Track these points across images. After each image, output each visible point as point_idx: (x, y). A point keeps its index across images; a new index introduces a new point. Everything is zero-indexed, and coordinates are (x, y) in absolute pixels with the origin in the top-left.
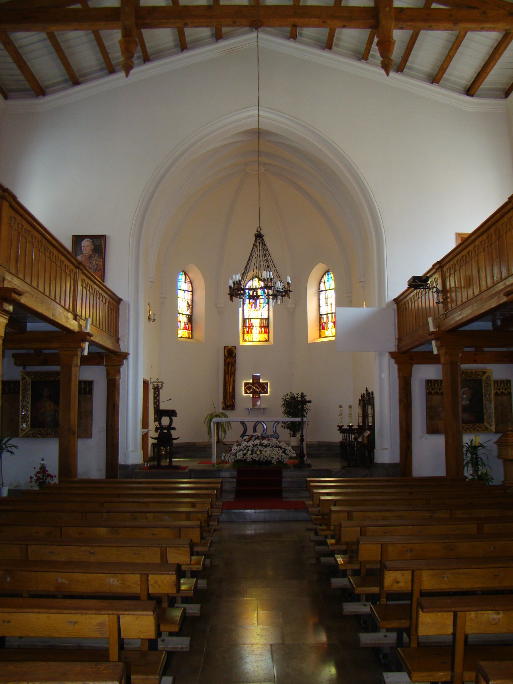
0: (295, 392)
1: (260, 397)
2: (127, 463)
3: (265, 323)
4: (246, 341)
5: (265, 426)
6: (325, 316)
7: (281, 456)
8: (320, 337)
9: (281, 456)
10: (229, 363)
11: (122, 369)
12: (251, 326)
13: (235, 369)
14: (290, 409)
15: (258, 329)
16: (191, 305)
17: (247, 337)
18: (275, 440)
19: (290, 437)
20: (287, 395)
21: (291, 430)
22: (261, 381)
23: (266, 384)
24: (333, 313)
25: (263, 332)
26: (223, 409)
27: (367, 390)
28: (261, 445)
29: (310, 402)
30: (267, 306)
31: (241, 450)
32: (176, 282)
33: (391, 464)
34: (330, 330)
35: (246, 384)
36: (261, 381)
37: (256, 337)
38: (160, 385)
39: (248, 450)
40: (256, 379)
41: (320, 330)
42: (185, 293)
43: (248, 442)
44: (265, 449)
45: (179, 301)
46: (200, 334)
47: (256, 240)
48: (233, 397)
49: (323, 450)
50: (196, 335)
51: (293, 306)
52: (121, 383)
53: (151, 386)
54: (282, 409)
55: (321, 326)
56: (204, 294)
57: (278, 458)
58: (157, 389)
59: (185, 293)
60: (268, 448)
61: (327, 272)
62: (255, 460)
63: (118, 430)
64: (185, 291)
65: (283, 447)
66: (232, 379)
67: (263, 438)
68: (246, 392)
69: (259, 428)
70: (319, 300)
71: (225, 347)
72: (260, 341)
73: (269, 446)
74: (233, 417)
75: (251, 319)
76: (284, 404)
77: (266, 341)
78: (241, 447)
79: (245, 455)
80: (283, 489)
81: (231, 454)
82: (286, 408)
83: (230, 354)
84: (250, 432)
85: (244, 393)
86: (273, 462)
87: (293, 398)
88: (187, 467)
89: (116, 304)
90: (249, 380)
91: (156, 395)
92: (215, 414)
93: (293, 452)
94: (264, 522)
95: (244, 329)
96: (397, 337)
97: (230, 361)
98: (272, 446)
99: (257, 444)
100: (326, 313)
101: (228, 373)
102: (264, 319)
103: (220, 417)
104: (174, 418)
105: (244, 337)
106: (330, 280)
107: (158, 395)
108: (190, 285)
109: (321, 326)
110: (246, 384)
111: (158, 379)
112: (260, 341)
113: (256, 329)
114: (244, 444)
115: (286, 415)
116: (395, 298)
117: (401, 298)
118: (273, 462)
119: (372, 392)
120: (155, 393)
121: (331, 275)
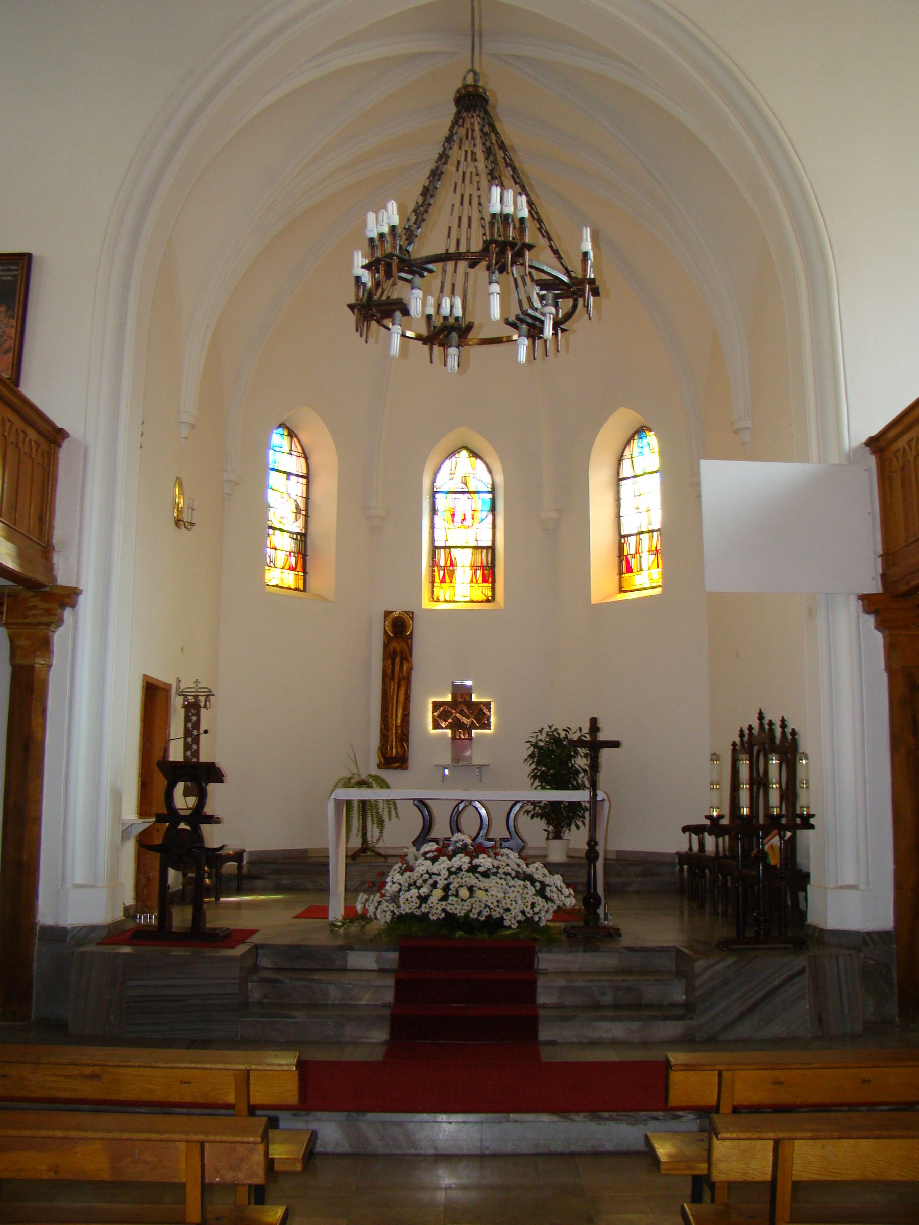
0: (560, 726)
1: (470, 738)
2: (62, 923)
3: (483, 558)
4: (438, 601)
5: (483, 812)
6: (632, 540)
7: (533, 905)
8: (621, 590)
9: (533, 905)
10: (395, 652)
11: (58, 638)
12: (452, 564)
13: (410, 669)
14: (549, 770)
15: (469, 573)
16: (306, 510)
17: (442, 591)
18: (514, 856)
19: (548, 838)
20: (541, 732)
21: (549, 823)
22: (474, 699)
23: (487, 705)
24: (652, 531)
25: (480, 580)
26: (379, 766)
27: (761, 716)
28: (473, 869)
29: (616, 744)
30: (490, 517)
31: (413, 884)
32: (266, 445)
33: (868, 933)
34: (645, 573)
35: (437, 705)
36: (474, 699)
37: (463, 590)
38: (202, 699)
39: (434, 885)
40: (462, 696)
41: (620, 573)
42: (288, 479)
43: (434, 860)
44: (484, 883)
45: (272, 497)
46: (324, 579)
47: (457, 121)
48: (404, 737)
49: (641, 875)
50: (313, 584)
51: (553, 515)
52: (53, 676)
53: (177, 703)
54: (528, 768)
55: (624, 565)
56: (336, 484)
57: (523, 912)
58: (193, 709)
59: (288, 479)
60: (493, 880)
61: (640, 431)
62: (454, 915)
63: (38, 819)
64: (289, 474)
65: (536, 876)
66: (402, 693)
67: (480, 850)
68: (437, 726)
69: (470, 825)
70: (618, 500)
71: (387, 614)
72: (472, 601)
73: (495, 874)
74: (402, 788)
75: (450, 547)
76: (532, 756)
77: (487, 601)
78: (414, 875)
79: (423, 899)
80: (541, 1012)
81: (383, 896)
82: (538, 764)
83: (399, 632)
84: (441, 829)
85: (430, 726)
86: (507, 923)
87: (555, 740)
88: (252, 932)
89: (44, 445)
90: (445, 695)
91: (190, 725)
92: (356, 779)
93: (566, 891)
94: (481, 1157)
95: (434, 571)
96: (881, 552)
97: (398, 648)
98: (506, 874)
99: (460, 869)
100: (635, 532)
101: (392, 679)
102: (482, 548)
103: (369, 786)
104: (212, 788)
105: (433, 592)
106: (646, 450)
107: (197, 725)
108: (303, 460)
109: (624, 565)
110: (437, 705)
111: (197, 682)
112: (472, 601)
113: (463, 574)
114: (423, 866)
115: (537, 783)
116: (874, 432)
117: (891, 434)
118: (507, 923)
119: (783, 720)
120: (187, 719)
121: (651, 439)
